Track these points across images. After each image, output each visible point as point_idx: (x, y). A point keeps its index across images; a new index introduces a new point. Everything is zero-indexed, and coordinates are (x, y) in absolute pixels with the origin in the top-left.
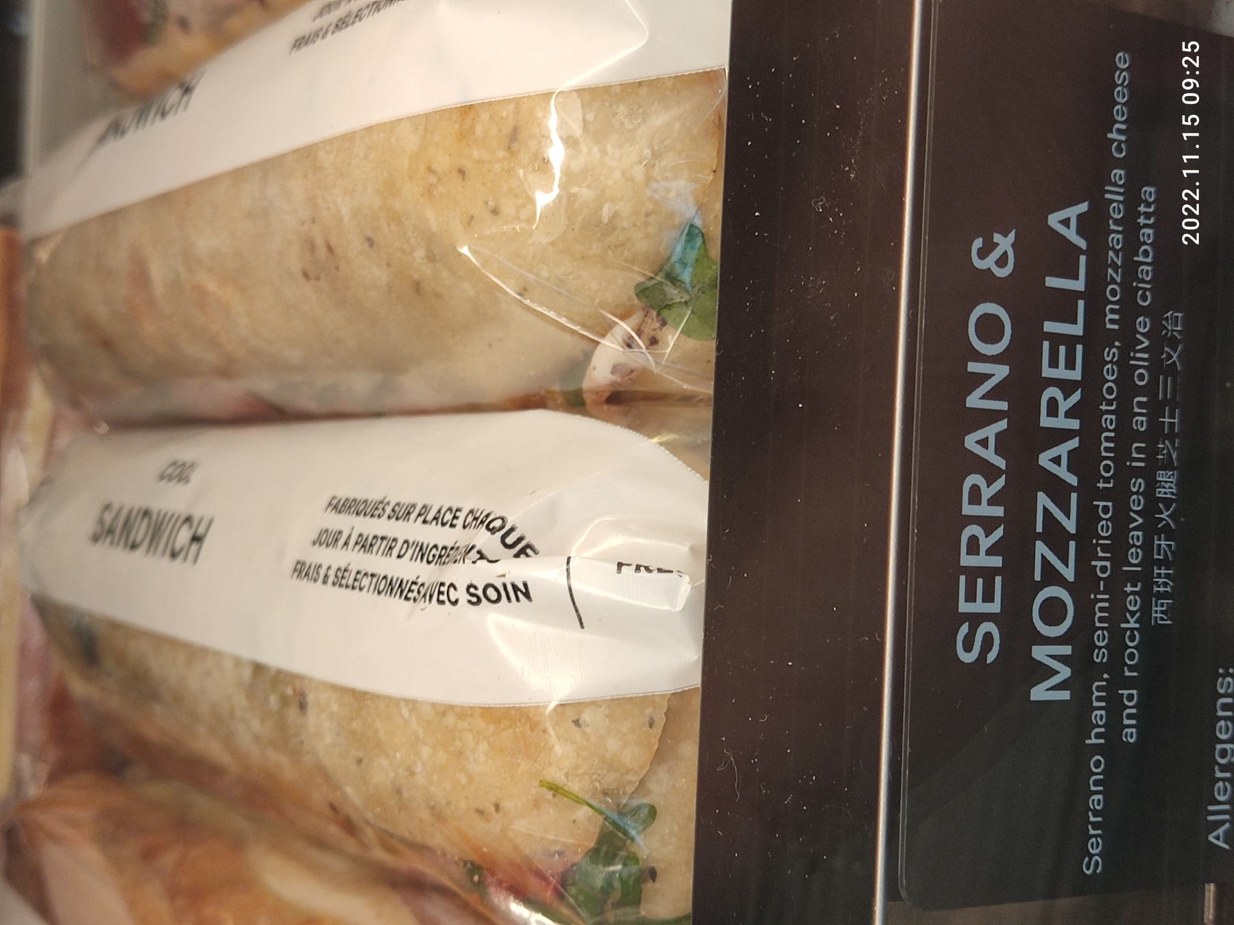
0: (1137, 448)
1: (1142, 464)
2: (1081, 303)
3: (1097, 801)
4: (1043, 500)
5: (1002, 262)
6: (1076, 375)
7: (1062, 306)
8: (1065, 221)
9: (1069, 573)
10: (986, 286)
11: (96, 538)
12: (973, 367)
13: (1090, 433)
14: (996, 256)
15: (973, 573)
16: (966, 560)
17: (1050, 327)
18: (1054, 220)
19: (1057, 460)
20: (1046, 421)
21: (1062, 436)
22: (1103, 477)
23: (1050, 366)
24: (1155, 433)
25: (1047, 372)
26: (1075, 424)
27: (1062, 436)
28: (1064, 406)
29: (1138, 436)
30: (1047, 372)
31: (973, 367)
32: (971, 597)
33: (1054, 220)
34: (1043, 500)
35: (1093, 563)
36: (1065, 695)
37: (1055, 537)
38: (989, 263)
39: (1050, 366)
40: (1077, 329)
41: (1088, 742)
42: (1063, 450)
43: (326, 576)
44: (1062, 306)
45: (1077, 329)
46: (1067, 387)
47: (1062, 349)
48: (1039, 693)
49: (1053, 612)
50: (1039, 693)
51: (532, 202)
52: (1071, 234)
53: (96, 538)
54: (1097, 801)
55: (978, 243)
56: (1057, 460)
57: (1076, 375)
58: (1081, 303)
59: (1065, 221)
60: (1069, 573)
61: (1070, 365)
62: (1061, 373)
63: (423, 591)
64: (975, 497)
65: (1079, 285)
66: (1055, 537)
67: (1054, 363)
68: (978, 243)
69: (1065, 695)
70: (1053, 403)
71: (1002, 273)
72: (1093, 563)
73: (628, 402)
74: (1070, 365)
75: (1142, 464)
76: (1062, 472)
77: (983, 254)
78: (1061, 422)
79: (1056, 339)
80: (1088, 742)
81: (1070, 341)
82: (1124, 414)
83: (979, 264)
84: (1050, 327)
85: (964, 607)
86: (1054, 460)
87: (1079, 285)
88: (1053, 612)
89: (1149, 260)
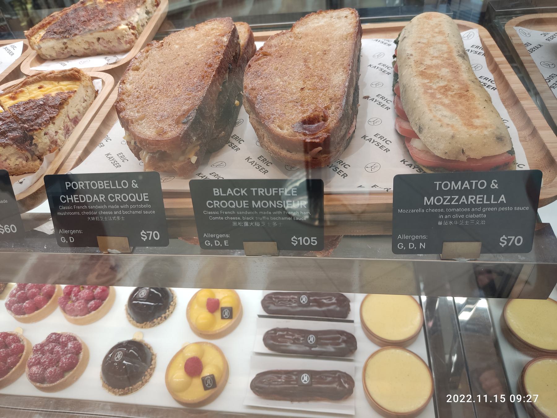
1: (221, 189)
3: (413, 211)
4: (457, 197)
5: (493, 186)
6: (477, 203)
7: (489, 199)
8: (503, 198)
9: (445, 203)
10: (489, 183)
12: (452, 189)
13: (467, 206)
14: (494, 186)
15: (278, 190)
17: (485, 196)
18: (503, 196)
20: (470, 197)
21: (467, 200)
24: (453, 220)
25: (478, 196)
26: (469, 203)
27: (467, 200)
28: (472, 200)
30: (478, 196)
31: (452, 189)
33: (503, 196)
34: (457, 197)
36: (425, 204)
37: (451, 200)
38: (493, 184)
40: (485, 202)
42: (465, 201)
44: (489, 199)
45: (485, 202)
46: (475, 201)
48: (426, 198)
49: (439, 200)
50: (426, 198)
51: (66, 287)
52: (501, 200)
54: (413, 211)
55: (496, 181)
57: (477, 203)
59: (503, 198)
60: (445, 203)
62: (478, 199)
63: (113, 161)
65: (492, 202)
66: (451, 200)
67: (479, 198)
68: (496, 181)
69: (425, 204)
71: (215, 195)
73: (388, 73)
75: (221, 189)
76: (461, 201)
77: (494, 182)
78: (470, 200)
79: (483, 198)
81: (483, 201)
82: (460, 213)
84: (485, 196)
86: (463, 199)
87: (492, 202)
88: (439, 200)
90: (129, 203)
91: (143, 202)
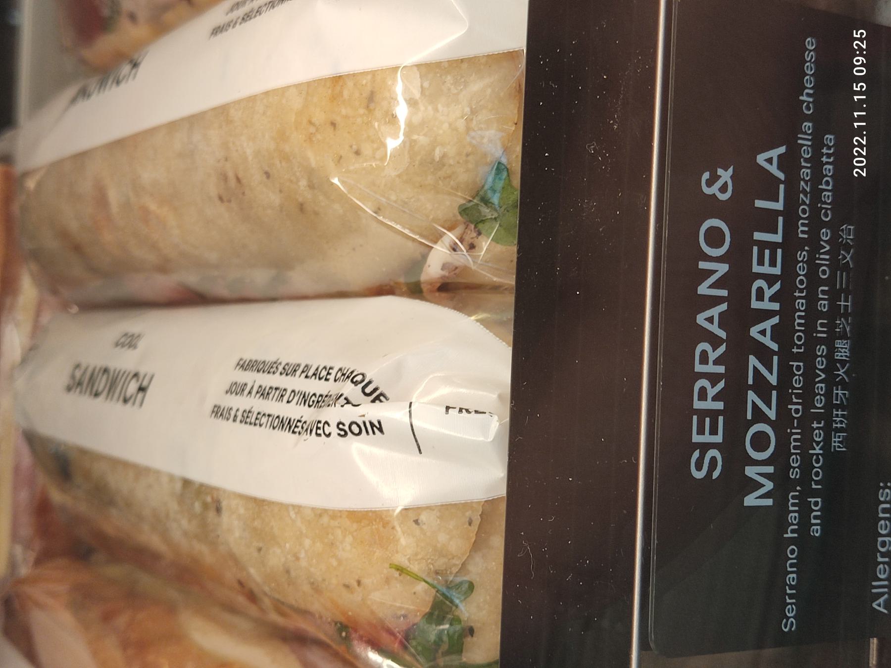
0: (821, 323)
1: (825, 335)
2: (781, 219)
3: (792, 579)
4: (753, 361)
5: (723, 189)
6: (777, 271)
7: (767, 221)
8: (769, 160)
9: (772, 414)
10: (712, 207)
11: (69, 389)
12: (703, 265)
13: (787, 313)
14: (719, 185)
15: (703, 414)
16: (698, 405)
17: (758, 236)
18: (761, 159)
19: (763, 332)
20: (755, 304)
21: (767, 315)
22: (797, 345)
23: (758, 264)
24: (834, 312)
25: (756, 269)
26: (776, 306)
27: (767, 315)
28: (768, 293)
29: (821, 315)
30: (756, 269)
31: (703, 265)
32: (701, 431)
33: (761, 159)
34: (753, 361)
35: (789, 407)
36: (769, 502)
37: (762, 387)
38: (714, 190)
39: (758, 264)
40: (778, 238)
41: (785, 536)
42: (767, 325)
43: (235, 416)
44: (767, 221)
45: (778, 238)
46: (770, 280)
47: (767, 252)
48: (750, 500)
49: (760, 442)
50: (750, 500)
52: (774, 169)
53: (69, 389)
54: (792, 579)
55: (706, 176)
56: (763, 332)
57: (777, 271)
58: (781, 219)
59: (769, 160)
60: (772, 414)
61: (773, 263)
62: (766, 269)
63: (305, 427)
64: (704, 359)
65: (779, 206)
66: (762, 387)
67: (761, 262)
68: (706, 176)
69: (769, 502)
70: (760, 291)
71: (723, 197)
72: (789, 407)
74: (773, 263)
75: (825, 335)
76: (767, 341)
77: (710, 183)
78: (766, 305)
79: (763, 245)
80: (785, 536)
81: (773, 246)
82: (812, 299)
83: (707, 190)
84: (758, 236)
85: (696, 438)
86: (761, 332)
87: (779, 206)
88: (760, 442)
89: (830, 188)
90: (782, 423)
91: (788, 163)
